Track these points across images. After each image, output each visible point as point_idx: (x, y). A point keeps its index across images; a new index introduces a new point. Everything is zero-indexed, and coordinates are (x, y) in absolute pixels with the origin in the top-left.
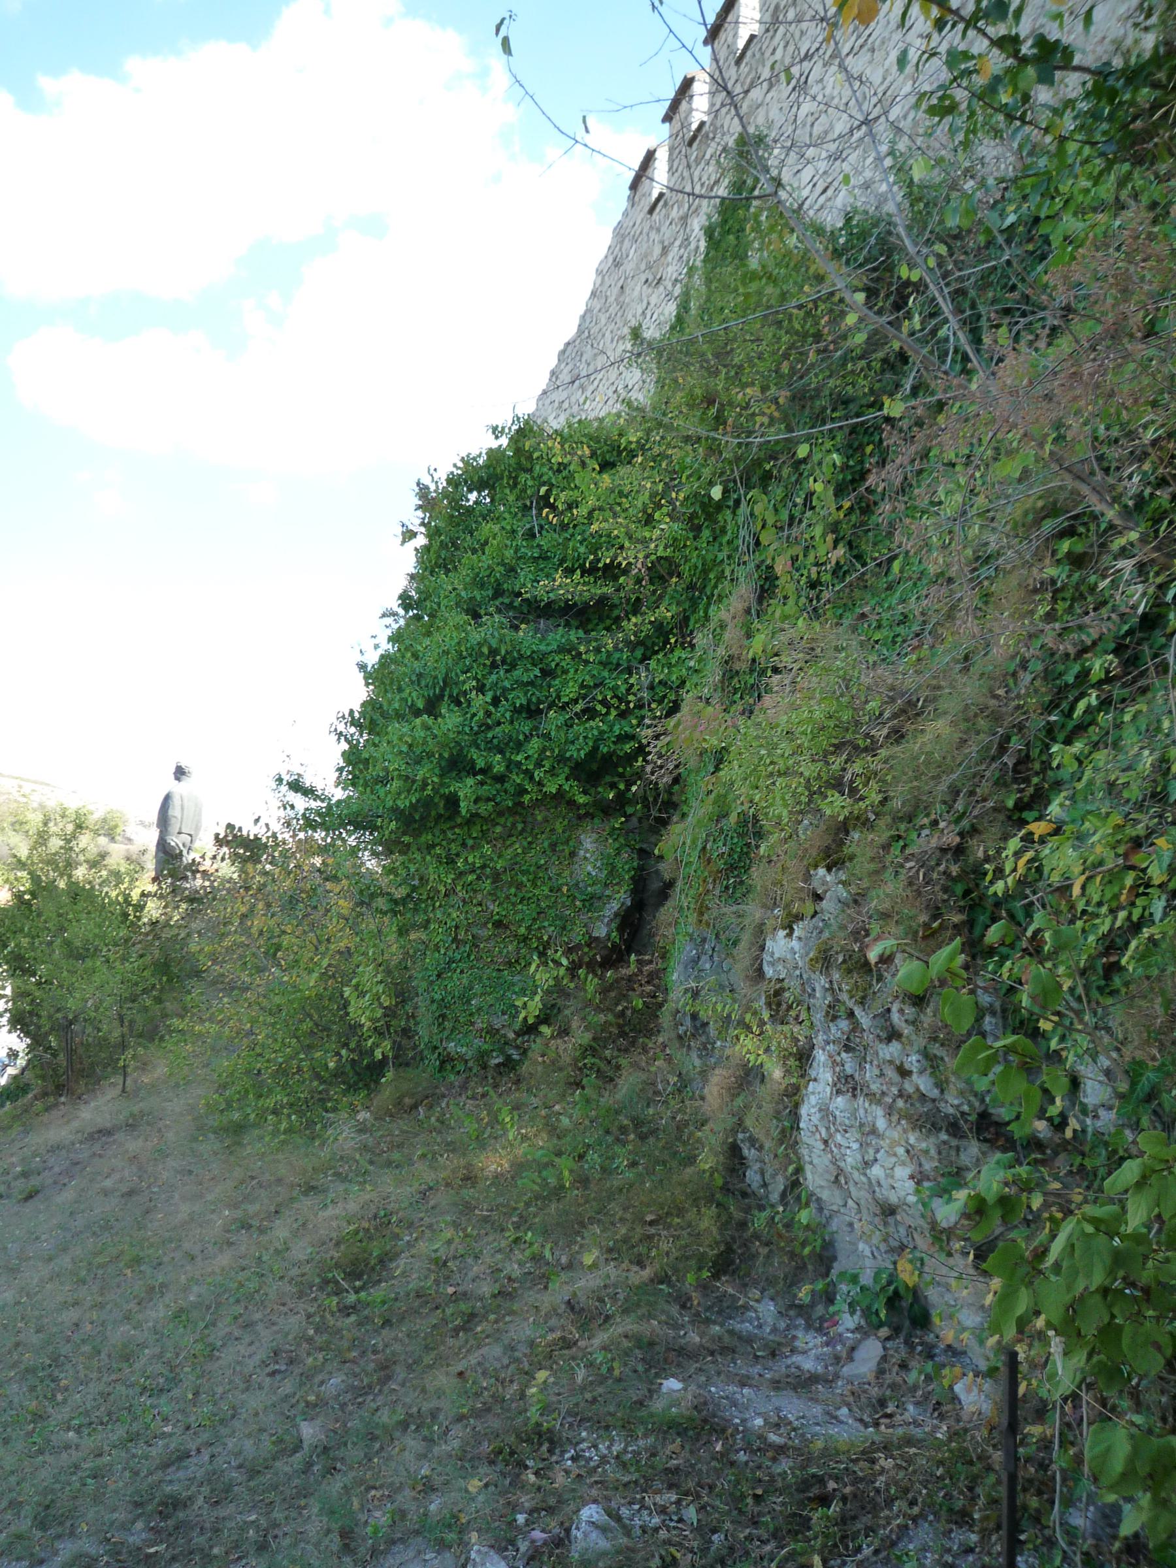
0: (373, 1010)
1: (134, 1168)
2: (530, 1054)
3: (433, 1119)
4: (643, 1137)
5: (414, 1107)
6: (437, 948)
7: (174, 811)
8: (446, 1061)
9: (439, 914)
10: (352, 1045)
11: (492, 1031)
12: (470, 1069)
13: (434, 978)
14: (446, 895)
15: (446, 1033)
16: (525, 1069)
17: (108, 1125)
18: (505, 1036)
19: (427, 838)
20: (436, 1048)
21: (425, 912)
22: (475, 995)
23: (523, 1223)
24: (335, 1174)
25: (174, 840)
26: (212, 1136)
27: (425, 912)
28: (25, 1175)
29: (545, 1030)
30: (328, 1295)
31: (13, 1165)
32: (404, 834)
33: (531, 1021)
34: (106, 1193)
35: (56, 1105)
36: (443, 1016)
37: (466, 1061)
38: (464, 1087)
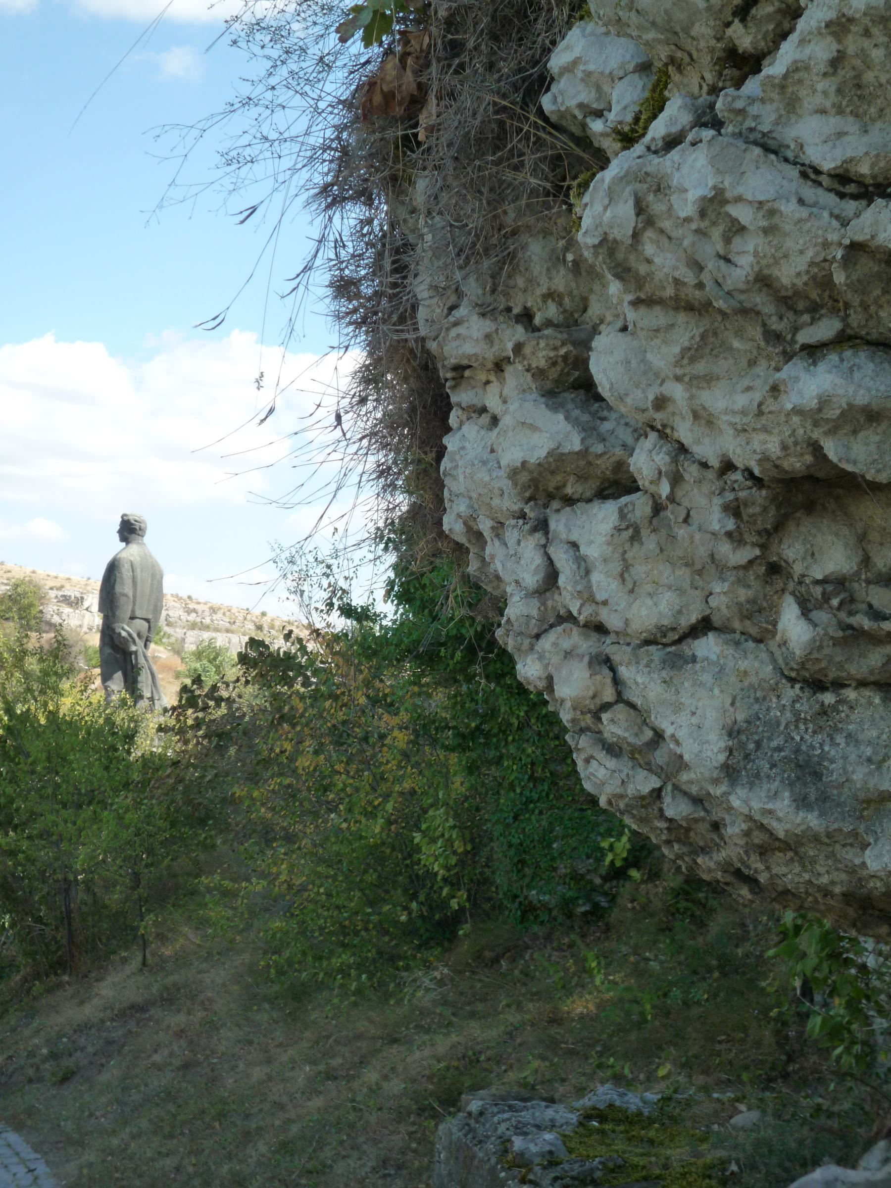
0: (447, 858)
1: (183, 1042)
2: (619, 901)
3: (517, 972)
4: (725, 975)
5: (496, 960)
6: (512, 787)
7: (124, 588)
8: (528, 911)
9: (512, 750)
10: (422, 898)
11: (576, 877)
12: (555, 919)
13: (510, 820)
14: (519, 728)
15: (527, 880)
16: (614, 916)
17: (140, 1000)
18: (591, 882)
20: (516, 896)
22: (556, 837)
23: (607, 1050)
24: (417, 1027)
25: (125, 629)
26: (267, 1006)
27: (497, 748)
28: (54, 1056)
29: (634, 873)
30: (426, 1119)
31: (37, 1047)
33: (618, 864)
34: (159, 1068)
35: (59, 986)
36: (523, 862)
37: (550, 910)
38: (548, 937)
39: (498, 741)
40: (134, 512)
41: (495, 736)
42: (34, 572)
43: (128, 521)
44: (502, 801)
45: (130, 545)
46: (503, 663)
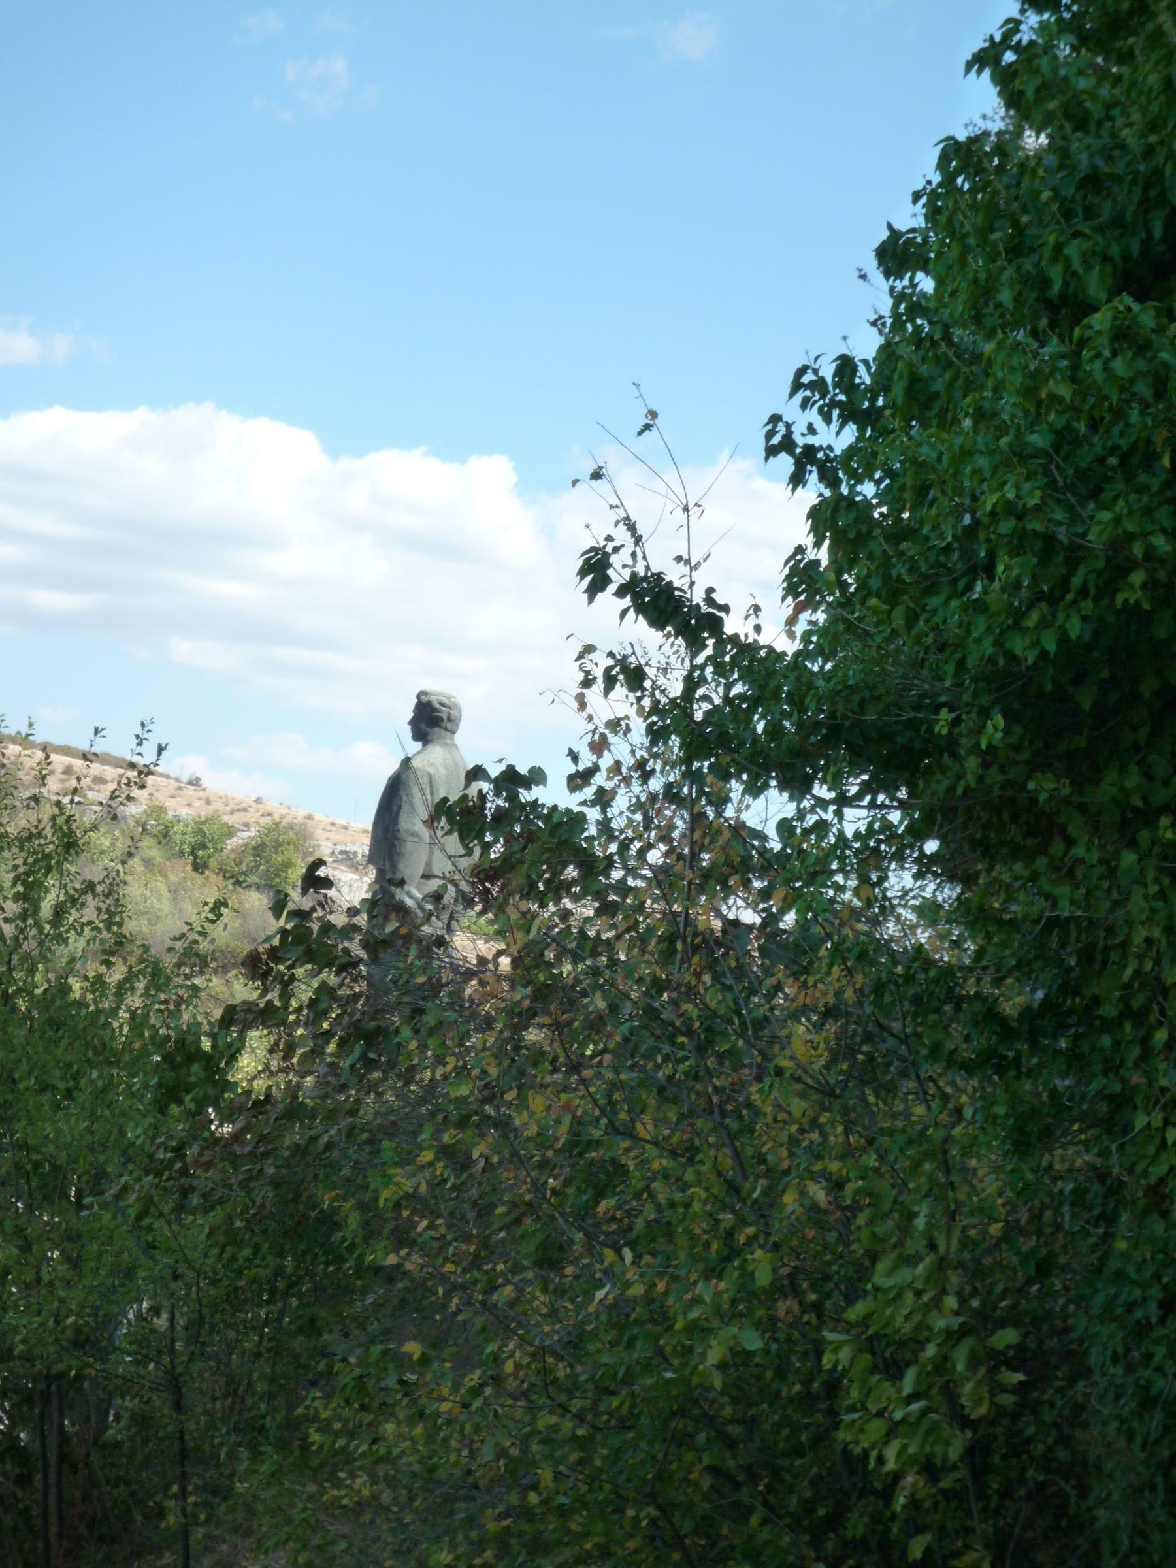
19: (1120, 784)
21: (1112, 1067)
32: (1036, 766)
39: (1117, 1044)
40: (438, 687)
41: (1109, 1026)
42: (310, 817)
43: (429, 704)
44: (1122, 1245)
45: (430, 747)
46: (1148, 776)
